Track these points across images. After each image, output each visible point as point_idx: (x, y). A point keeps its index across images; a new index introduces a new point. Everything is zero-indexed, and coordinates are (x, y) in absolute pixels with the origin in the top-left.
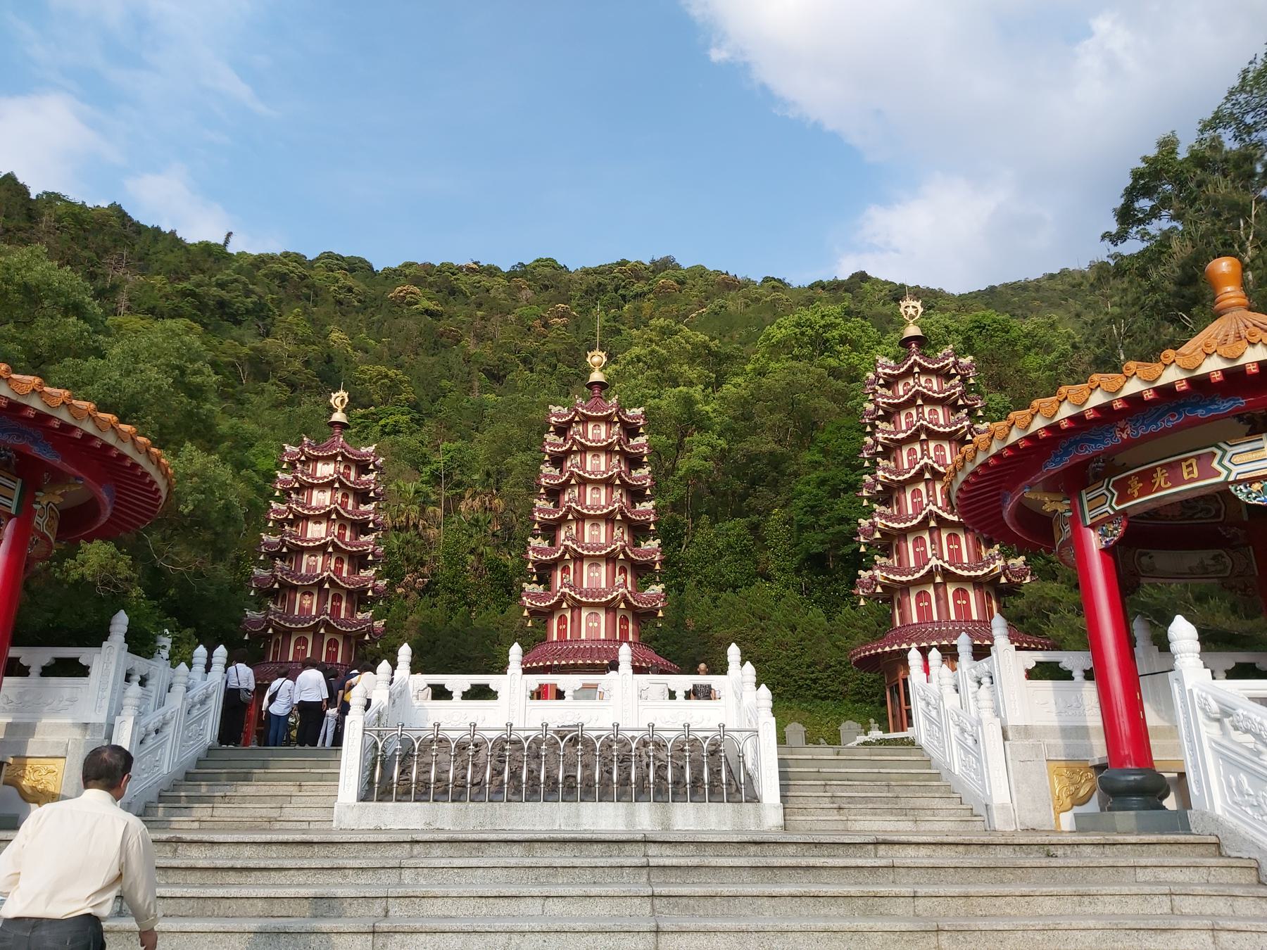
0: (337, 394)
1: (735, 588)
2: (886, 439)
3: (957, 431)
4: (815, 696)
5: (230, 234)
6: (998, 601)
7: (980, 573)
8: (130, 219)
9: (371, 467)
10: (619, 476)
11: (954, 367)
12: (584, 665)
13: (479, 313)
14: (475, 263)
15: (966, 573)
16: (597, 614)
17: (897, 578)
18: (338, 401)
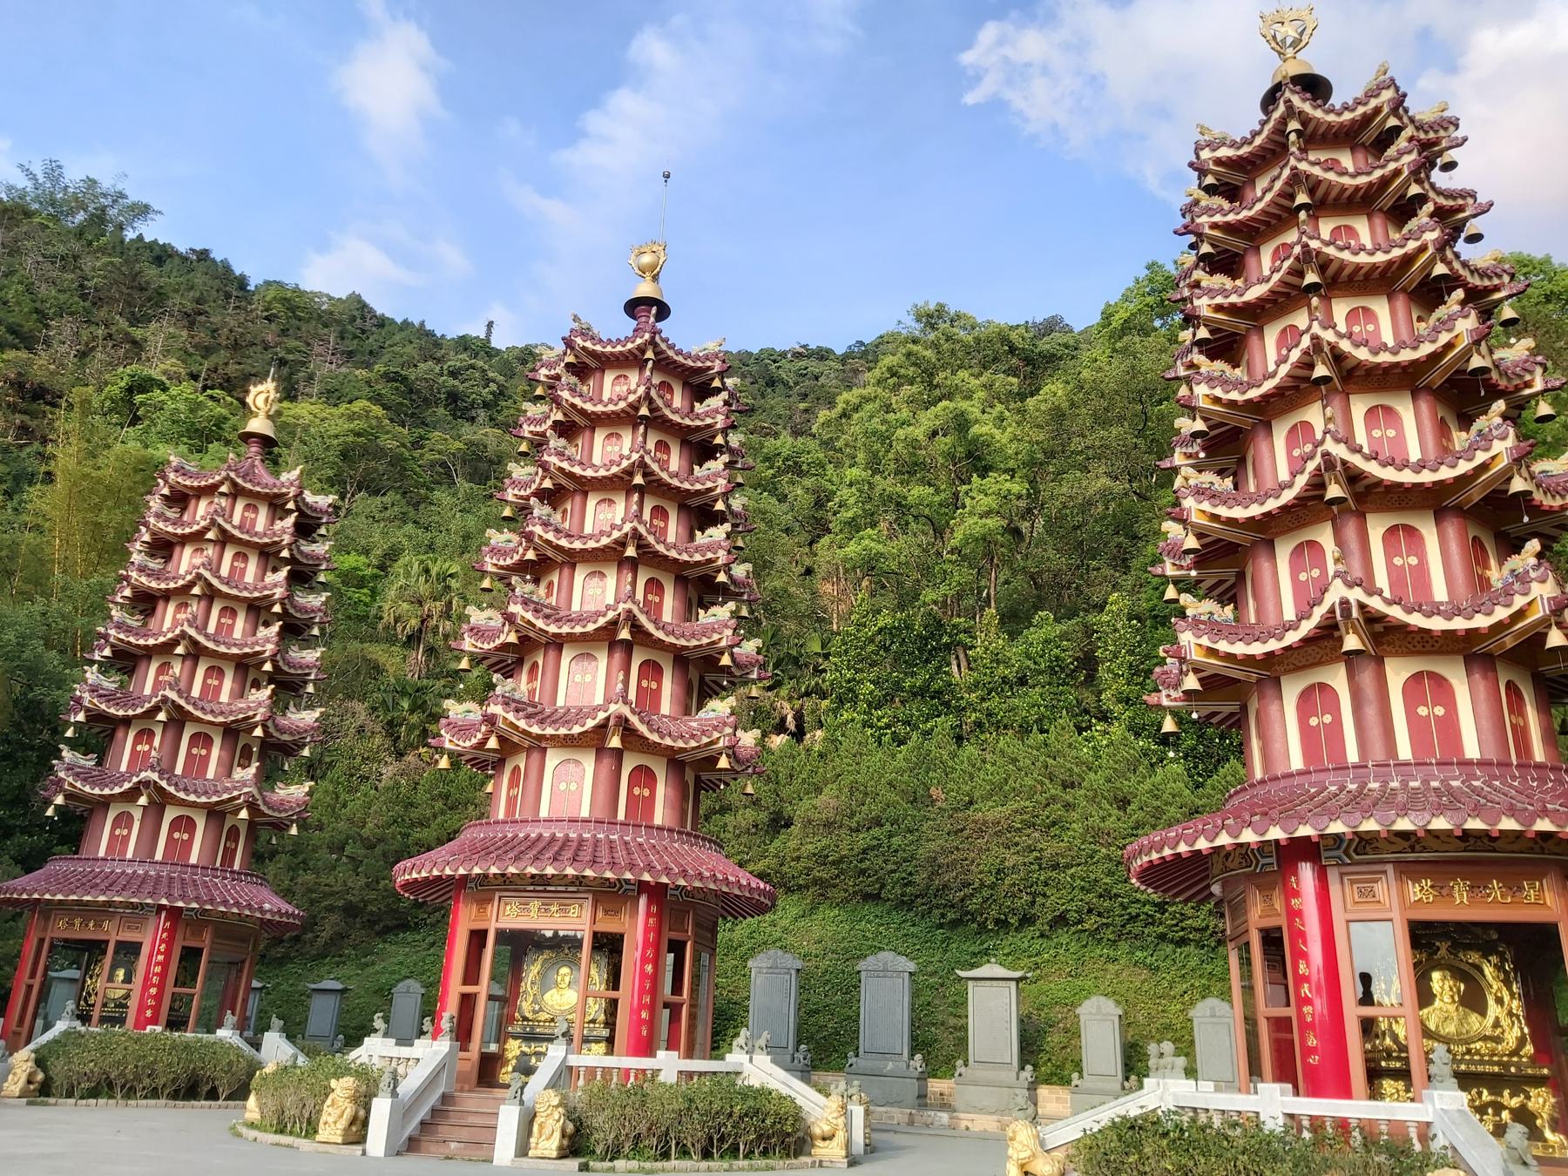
0: (260, 388)
1: (1024, 730)
2: (1219, 308)
3: (1408, 260)
4: (1162, 937)
5: (490, 325)
6: (1544, 707)
7: (1481, 622)
8: (371, 311)
9: (291, 505)
10: (642, 464)
11: (1394, 111)
12: (561, 879)
13: (802, 406)
14: (804, 347)
15: (1437, 624)
16: (577, 762)
17: (1239, 649)
18: (260, 401)
